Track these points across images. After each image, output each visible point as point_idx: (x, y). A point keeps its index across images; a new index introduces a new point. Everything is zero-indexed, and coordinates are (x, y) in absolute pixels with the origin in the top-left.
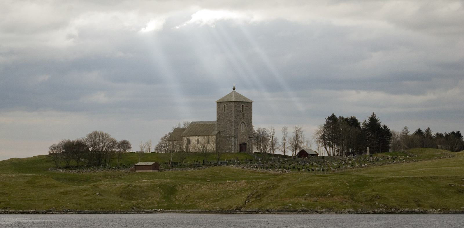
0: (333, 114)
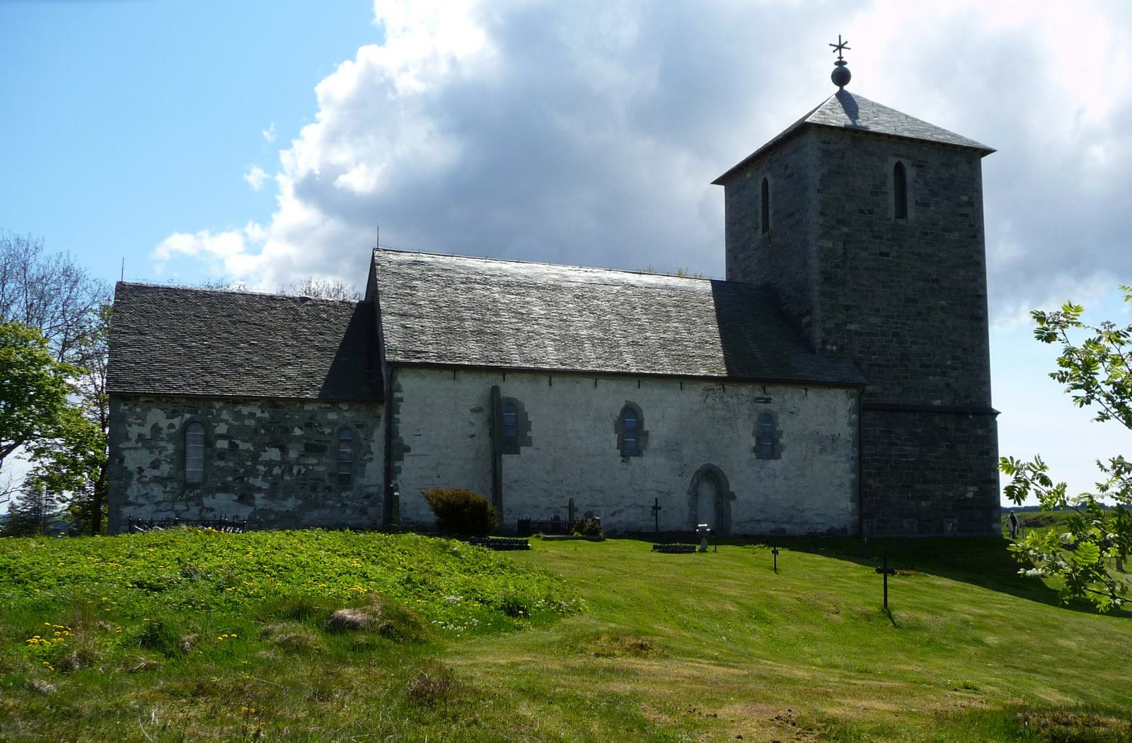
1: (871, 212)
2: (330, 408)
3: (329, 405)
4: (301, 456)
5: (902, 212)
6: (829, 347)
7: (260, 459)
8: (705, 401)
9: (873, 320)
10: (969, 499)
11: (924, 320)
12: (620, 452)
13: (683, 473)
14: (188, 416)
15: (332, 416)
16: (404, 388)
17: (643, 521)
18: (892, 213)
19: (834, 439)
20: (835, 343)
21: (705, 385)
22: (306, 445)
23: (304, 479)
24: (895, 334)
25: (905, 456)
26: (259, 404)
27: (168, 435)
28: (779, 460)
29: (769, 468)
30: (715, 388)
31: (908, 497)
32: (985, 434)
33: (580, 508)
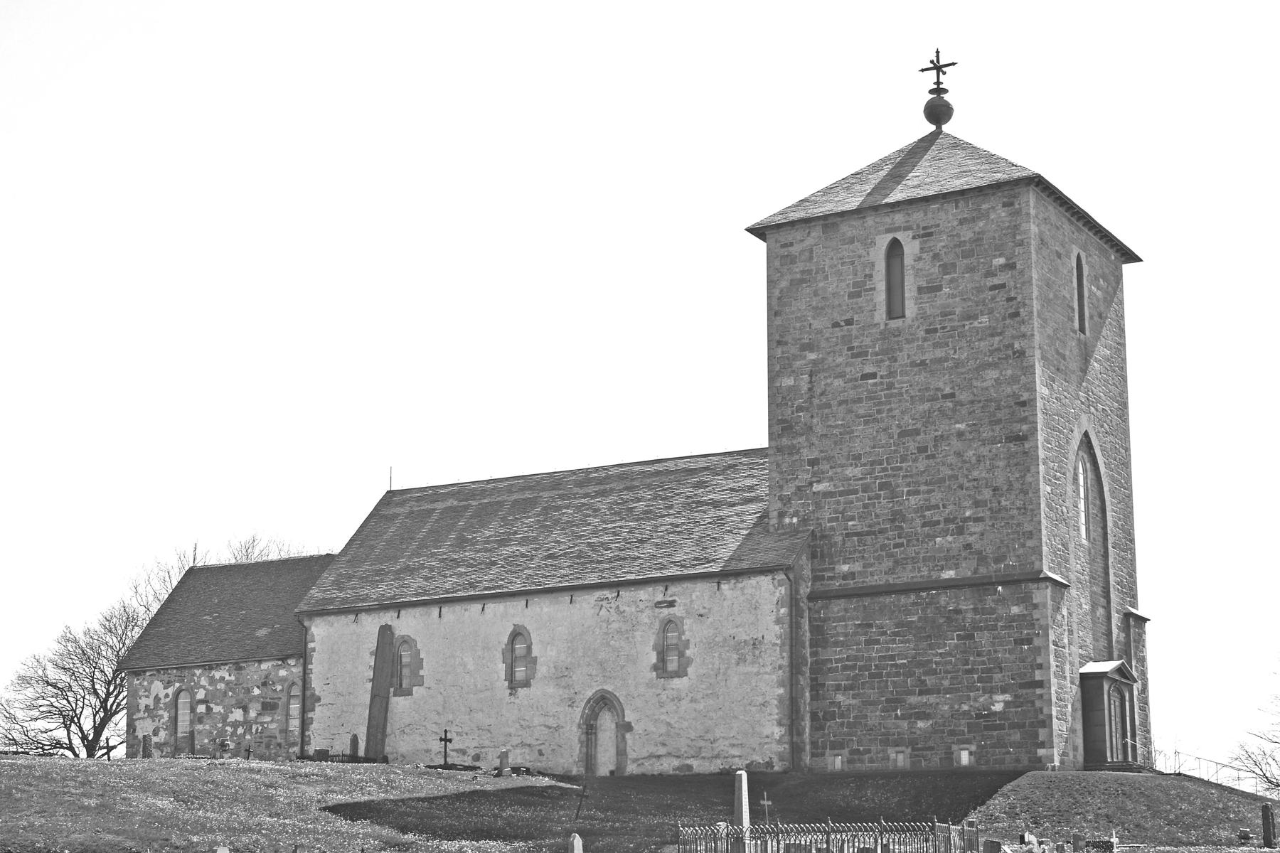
0: (758, 231)
1: (849, 322)
2: (281, 665)
3: (280, 663)
4: (259, 714)
5: (895, 310)
6: (787, 520)
7: (228, 720)
8: (598, 615)
9: (849, 472)
10: (995, 713)
11: (928, 457)
12: (507, 684)
13: (573, 703)
14: (177, 685)
15: (282, 673)
16: (317, 638)
17: (530, 762)
18: (880, 315)
19: (756, 644)
20: (796, 514)
21: (598, 594)
22: (263, 703)
23: (261, 738)
24: (882, 486)
25: (892, 658)
26: (227, 667)
27: (165, 704)
28: (685, 677)
29: (673, 689)
30: (610, 597)
31: (896, 715)
32: (1025, 612)
33: (468, 750)
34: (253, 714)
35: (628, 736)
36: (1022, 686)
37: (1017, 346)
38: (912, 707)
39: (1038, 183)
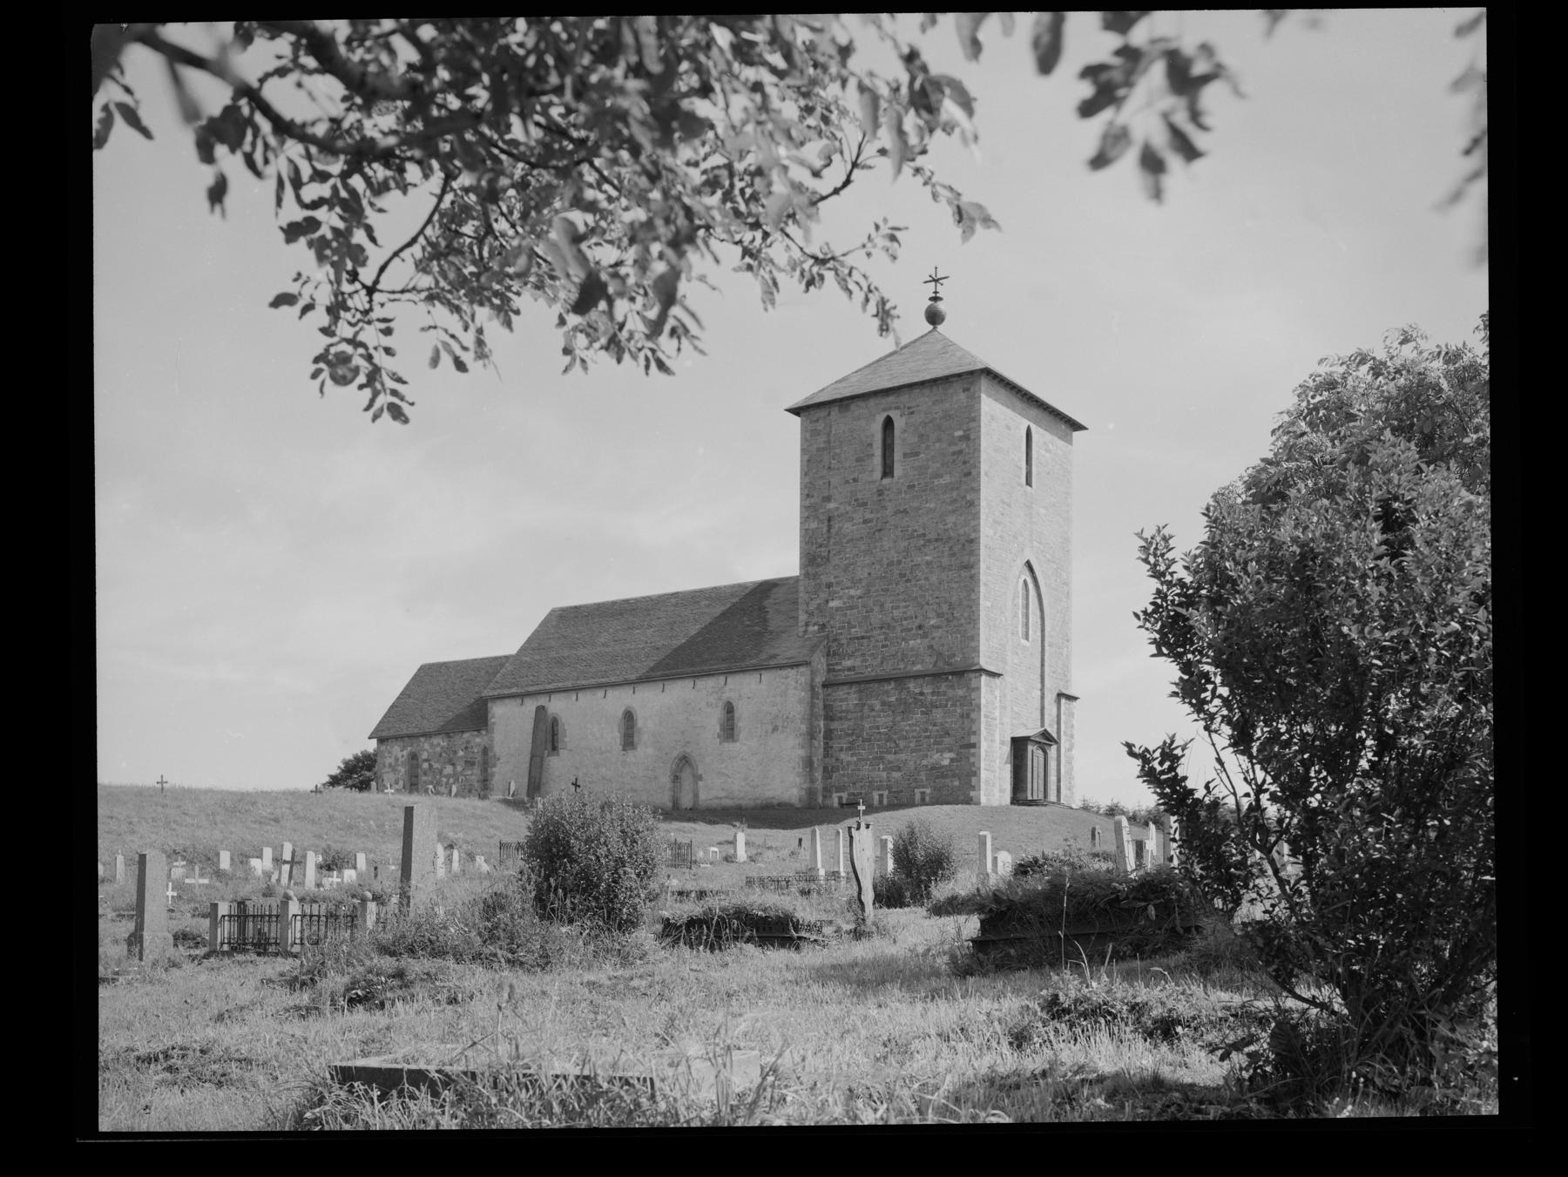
0: (796, 411)
5: (888, 471)
9: (852, 592)
15: (478, 740)
18: (878, 474)
34: (459, 769)
35: (700, 783)
36: (962, 747)
37: (968, 498)
38: (890, 762)
39: (988, 372)
